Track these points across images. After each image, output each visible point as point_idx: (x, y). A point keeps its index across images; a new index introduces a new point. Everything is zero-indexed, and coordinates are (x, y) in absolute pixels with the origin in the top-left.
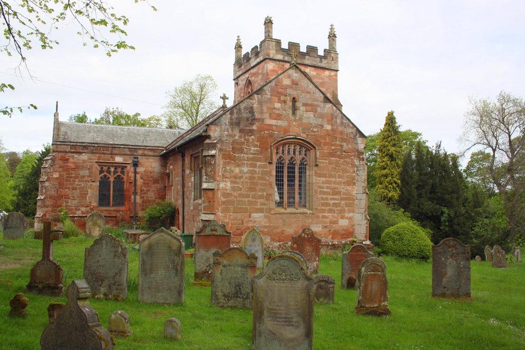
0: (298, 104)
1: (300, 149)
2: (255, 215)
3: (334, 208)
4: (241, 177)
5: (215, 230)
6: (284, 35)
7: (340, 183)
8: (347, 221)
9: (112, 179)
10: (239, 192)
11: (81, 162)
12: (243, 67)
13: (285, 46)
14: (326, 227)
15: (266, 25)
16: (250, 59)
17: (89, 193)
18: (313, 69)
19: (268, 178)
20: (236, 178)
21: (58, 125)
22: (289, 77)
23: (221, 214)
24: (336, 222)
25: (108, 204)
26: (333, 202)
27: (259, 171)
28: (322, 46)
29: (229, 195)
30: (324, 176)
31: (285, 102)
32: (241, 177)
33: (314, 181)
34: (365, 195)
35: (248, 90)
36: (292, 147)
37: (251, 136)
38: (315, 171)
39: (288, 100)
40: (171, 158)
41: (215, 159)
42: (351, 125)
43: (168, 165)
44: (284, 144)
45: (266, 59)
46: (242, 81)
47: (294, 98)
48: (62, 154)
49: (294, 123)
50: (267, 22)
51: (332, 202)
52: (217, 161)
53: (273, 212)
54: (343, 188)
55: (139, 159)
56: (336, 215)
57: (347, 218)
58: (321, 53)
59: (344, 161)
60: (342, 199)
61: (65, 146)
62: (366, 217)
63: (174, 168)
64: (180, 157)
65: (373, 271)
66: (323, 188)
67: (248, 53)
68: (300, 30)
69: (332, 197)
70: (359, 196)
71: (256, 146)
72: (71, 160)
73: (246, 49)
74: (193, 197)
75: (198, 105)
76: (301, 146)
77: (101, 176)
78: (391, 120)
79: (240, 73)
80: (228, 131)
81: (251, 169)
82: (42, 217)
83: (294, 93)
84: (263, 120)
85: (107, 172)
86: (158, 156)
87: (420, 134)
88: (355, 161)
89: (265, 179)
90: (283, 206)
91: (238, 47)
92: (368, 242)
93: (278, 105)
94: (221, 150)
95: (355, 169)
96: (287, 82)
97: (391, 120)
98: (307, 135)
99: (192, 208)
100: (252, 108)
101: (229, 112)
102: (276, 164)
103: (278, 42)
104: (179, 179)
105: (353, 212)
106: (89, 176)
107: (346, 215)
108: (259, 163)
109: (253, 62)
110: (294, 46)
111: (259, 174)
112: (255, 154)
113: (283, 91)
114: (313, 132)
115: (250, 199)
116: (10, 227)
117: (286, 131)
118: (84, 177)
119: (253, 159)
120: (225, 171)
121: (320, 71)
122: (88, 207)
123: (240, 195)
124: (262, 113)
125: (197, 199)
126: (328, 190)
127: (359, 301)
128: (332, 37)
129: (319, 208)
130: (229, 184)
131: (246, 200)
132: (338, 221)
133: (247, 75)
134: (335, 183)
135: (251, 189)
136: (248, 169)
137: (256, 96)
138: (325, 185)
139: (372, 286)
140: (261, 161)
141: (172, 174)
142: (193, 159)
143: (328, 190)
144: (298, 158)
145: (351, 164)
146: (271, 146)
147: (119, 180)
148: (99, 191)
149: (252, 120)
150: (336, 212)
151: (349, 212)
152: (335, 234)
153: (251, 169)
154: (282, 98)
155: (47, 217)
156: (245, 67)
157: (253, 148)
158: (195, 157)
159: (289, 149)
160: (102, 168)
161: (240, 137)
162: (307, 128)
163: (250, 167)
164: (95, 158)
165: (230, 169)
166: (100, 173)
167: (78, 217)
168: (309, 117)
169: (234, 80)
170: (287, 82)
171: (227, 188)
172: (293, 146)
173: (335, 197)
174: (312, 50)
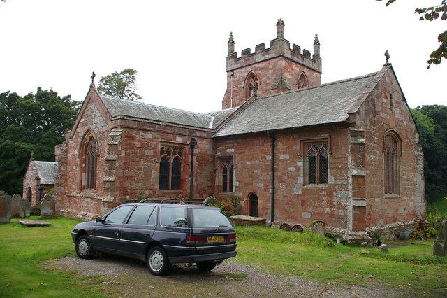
8: (152, 151)
25: (167, 188)
72: (138, 138)
78: (39, 89)
87: (70, 96)
91: (231, 42)
93: (385, 100)
97: (39, 89)
106: (153, 156)
121: (312, 72)
128: (317, 44)
142: (302, 147)
164: (159, 136)
166: (161, 154)
169: (227, 72)
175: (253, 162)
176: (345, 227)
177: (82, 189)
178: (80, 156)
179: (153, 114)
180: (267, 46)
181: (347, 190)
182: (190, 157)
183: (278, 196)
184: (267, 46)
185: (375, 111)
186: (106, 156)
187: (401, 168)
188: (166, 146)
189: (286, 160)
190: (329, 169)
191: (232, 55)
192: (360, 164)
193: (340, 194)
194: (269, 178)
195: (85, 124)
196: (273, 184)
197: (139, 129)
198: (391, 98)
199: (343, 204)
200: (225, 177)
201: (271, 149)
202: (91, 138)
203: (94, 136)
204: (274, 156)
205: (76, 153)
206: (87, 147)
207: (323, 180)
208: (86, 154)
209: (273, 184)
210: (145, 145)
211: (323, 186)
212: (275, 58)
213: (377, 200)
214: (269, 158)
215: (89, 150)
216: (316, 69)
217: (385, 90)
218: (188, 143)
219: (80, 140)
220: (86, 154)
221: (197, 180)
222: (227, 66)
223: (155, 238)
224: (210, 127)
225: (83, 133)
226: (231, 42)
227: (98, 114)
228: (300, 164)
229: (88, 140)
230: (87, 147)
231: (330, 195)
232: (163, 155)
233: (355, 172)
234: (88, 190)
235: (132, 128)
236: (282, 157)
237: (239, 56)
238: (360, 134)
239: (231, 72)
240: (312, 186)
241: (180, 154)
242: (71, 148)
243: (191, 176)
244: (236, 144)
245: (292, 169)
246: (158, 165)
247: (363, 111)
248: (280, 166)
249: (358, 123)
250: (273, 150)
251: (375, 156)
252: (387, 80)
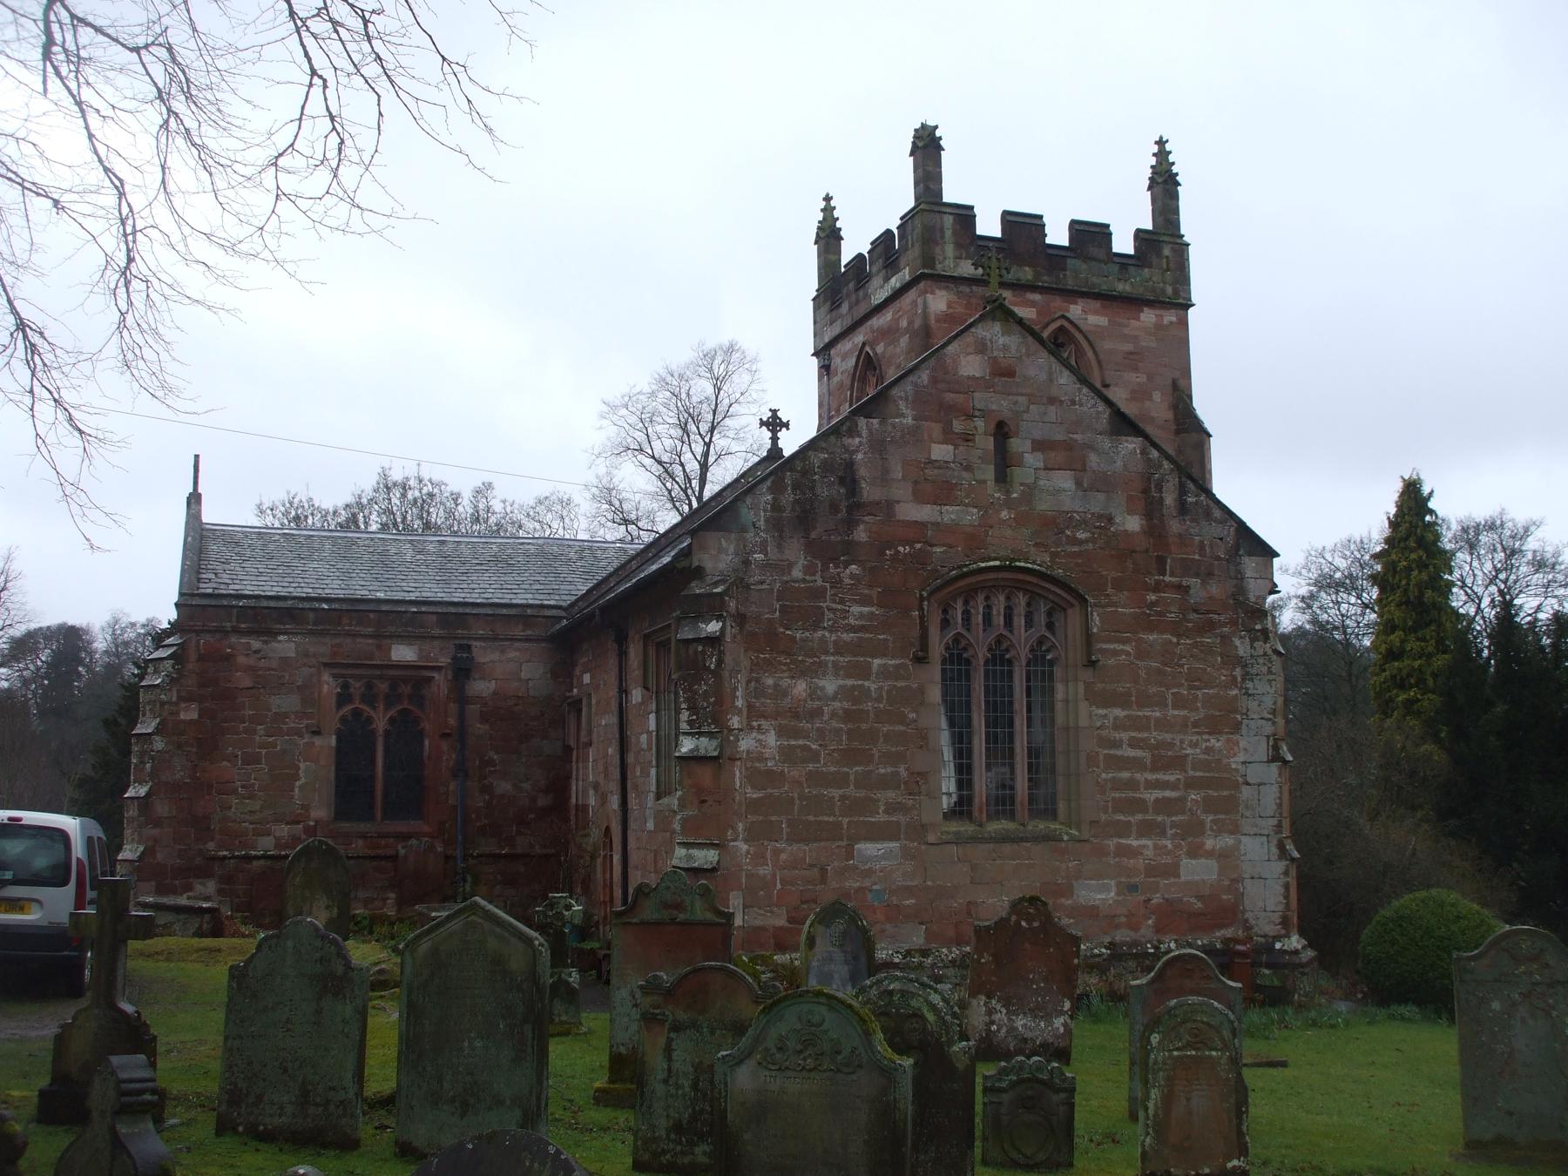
0: (1017, 444)
1: (1029, 605)
2: (868, 849)
3: (1160, 819)
4: (816, 713)
5: (679, 906)
6: (984, 190)
7: (1184, 726)
8: (1213, 864)
9: (381, 723)
10: (811, 767)
11: (274, 664)
12: (845, 308)
13: (988, 225)
14: (1133, 888)
15: (918, 153)
16: (869, 277)
17: (301, 774)
18: (1097, 304)
19: (912, 715)
20: (796, 716)
21: (202, 542)
22: (982, 348)
23: (745, 847)
24: (1173, 870)
26: (1158, 794)
27: (881, 688)
28: (1128, 221)
29: (772, 777)
30: (1122, 700)
31: (968, 438)
32: (816, 713)
33: (1083, 722)
34: (1274, 767)
35: (860, 384)
36: (999, 603)
37: (847, 564)
38: (1088, 685)
39: (981, 430)
40: (585, 647)
41: (721, 653)
42: (1217, 513)
43: (577, 672)
44: (969, 595)
45: (922, 277)
46: (845, 363)
47: (1001, 425)
48: (209, 637)
49: (1004, 514)
50: (920, 144)
51: (1151, 796)
52: (728, 659)
53: (931, 838)
54: (1193, 746)
55: (475, 652)
56: (1169, 844)
57: (1210, 854)
58: (1123, 244)
59: (1195, 645)
60: (1191, 784)
61: (232, 617)
62: (1281, 846)
63: (594, 680)
64: (612, 646)
65: (1188, 1046)
66: (1117, 744)
67: (860, 256)
68: (1047, 171)
69: (1151, 777)
70: (1254, 772)
71: (865, 601)
73: (855, 244)
74: (653, 788)
75: (708, 445)
76: (1033, 596)
77: (341, 713)
79: (836, 329)
80: (764, 551)
81: (850, 682)
82: (140, 858)
83: (1000, 405)
84: (889, 506)
85: (364, 699)
86: (543, 640)
88: (1237, 642)
89: (902, 719)
90: (970, 814)
91: (829, 236)
92: (1295, 942)
93: (941, 452)
94: (741, 619)
95: (1238, 672)
96: (971, 366)
98: (1054, 555)
99: (650, 825)
100: (850, 465)
101: (769, 483)
102: (944, 662)
103: (965, 215)
104: (609, 720)
105: (1235, 830)
107: (1209, 843)
108: (877, 662)
109: (879, 292)
110: (1023, 228)
111: (879, 700)
112: (861, 629)
113: (960, 398)
114: (1074, 541)
115: (851, 791)
117: (974, 541)
118: (281, 717)
119: (857, 648)
120: (760, 692)
122: (298, 823)
123: (811, 776)
124: (884, 478)
126: (1138, 753)
127: (1144, 1155)
128: (1164, 183)
129: (1103, 817)
130: (771, 739)
131: (836, 793)
132: (1176, 866)
133: (859, 338)
134: (1162, 724)
135: (850, 756)
136: (841, 682)
137: (862, 422)
138: (1125, 736)
139: (1188, 1100)
140: (884, 655)
141: (590, 705)
142: (652, 652)
143: (1138, 753)
144: (1022, 639)
145: (1221, 655)
146: (922, 599)
147: (406, 728)
148: (338, 769)
149: (850, 509)
150: (1170, 832)
151: (1219, 830)
152: (1170, 916)
153: (850, 682)
154: (958, 426)
155: (160, 857)
156: (851, 308)
157: (856, 609)
158: (659, 644)
159: (988, 607)
160: (345, 686)
161: (809, 570)
162: (1054, 525)
163: (848, 676)
164: (322, 648)
165: (776, 685)
166: (340, 705)
167: (263, 857)
168: (1060, 489)
169: (816, 354)
170: (971, 366)
171: (767, 752)
172: (1002, 598)
173: (1160, 776)
174: (1090, 235)
179: (383, 561)
188: (357, 678)
218: (444, 660)
232: (347, 708)
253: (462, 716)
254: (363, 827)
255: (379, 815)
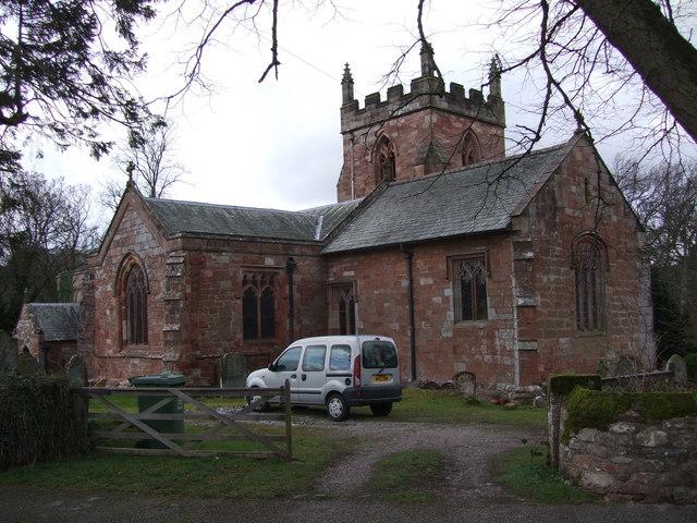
32: (549, 288)
42: (592, 159)
91: (348, 82)
93: (574, 189)
106: (233, 290)
116: (230, 378)
118: (225, 291)
125: (459, 321)
130: (538, 298)
142: (450, 263)
147: (268, 295)
164: (239, 258)
166: (243, 285)
169: (343, 133)
175: (382, 291)
176: (513, 382)
177: (122, 345)
178: (117, 293)
180: (407, 90)
181: (512, 327)
182: (287, 287)
183: (421, 342)
184: (407, 90)
185: (555, 208)
186: (160, 292)
187: (609, 289)
189: (430, 286)
190: (488, 298)
191: (349, 104)
192: (528, 290)
193: (505, 334)
194: (407, 313)
195: (122, 243)
196: (412, 323)
197: (210, 251)
198: (586, 184)
199: (508, 348)
200: (343, 315)
201: (405, 269)
202: (134, 265)
203: (140, 264)
204: (411, 281)
205: (109, 288)
206: (127, 278)
207: (482, 313)
208: (125, 290)
209: (412, 323)
210: (219, 274)
211: (481, 324)
212: (421, 110)
213: (562, 340)
214: (405, 283)
215: (130, 284)
216: (494, 119)
217: (574, 173)
218: (284, 265)
219: (115, 269)
220: (125, 290)
221: (299, 322)
222: (342, 124)
223: (538, 48)
224: (318, 238)
225: (120, 257)
226: (348, 82)
227: (144, 229)
228: (449, 292)
229: (128, 269)
230: (127, 278)
231: (491, 336)
233: (521, 302)
234: (134, 346)
235: (200, 250)
236: (423, 282)
237: (362, 106)
238: (528, 246)
239: (349, 134)
240: (467, 324)
241: (271, 283)
242: (100, 281)
243: (291, 315)
244: (356, 263)
245: (437, 300)
246: (240, 302)
247: (532, 211)
248: (420, 297)
249: (525, 230)
250: (410, 269)
251: (556, 277)
252: (579, 156)
253: (291, 290)
254: (255, 341)
255: (260, 334)
